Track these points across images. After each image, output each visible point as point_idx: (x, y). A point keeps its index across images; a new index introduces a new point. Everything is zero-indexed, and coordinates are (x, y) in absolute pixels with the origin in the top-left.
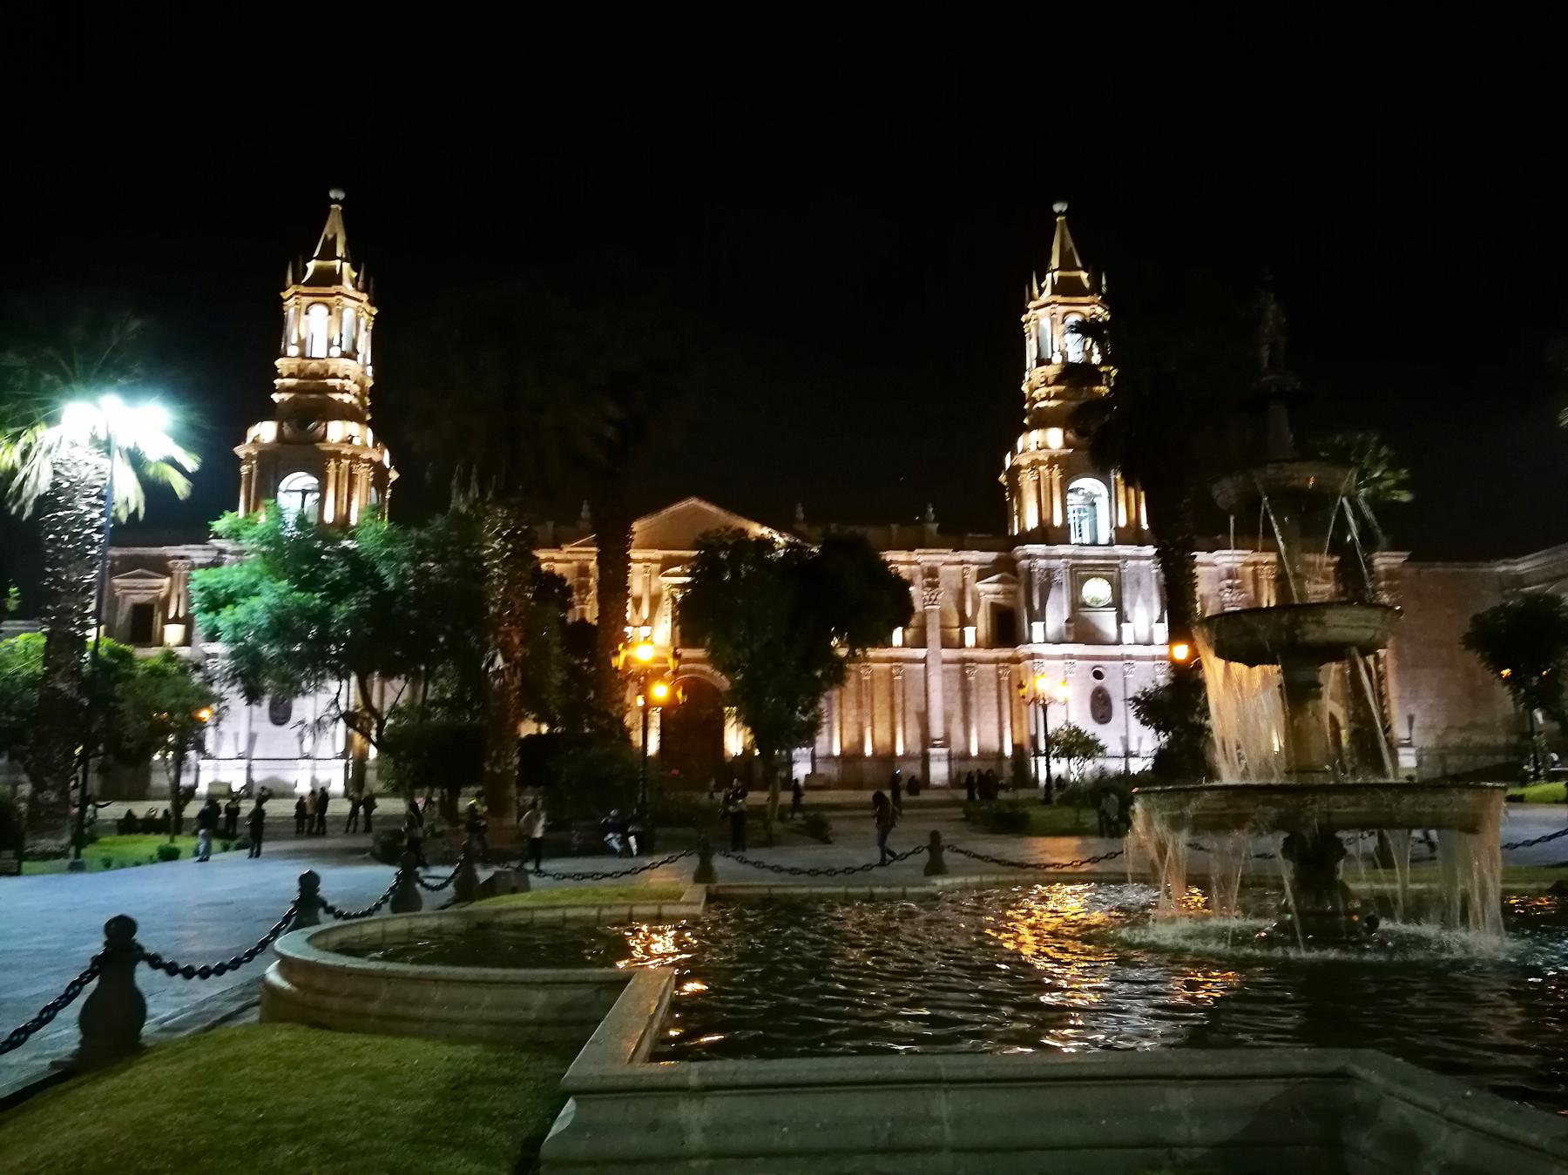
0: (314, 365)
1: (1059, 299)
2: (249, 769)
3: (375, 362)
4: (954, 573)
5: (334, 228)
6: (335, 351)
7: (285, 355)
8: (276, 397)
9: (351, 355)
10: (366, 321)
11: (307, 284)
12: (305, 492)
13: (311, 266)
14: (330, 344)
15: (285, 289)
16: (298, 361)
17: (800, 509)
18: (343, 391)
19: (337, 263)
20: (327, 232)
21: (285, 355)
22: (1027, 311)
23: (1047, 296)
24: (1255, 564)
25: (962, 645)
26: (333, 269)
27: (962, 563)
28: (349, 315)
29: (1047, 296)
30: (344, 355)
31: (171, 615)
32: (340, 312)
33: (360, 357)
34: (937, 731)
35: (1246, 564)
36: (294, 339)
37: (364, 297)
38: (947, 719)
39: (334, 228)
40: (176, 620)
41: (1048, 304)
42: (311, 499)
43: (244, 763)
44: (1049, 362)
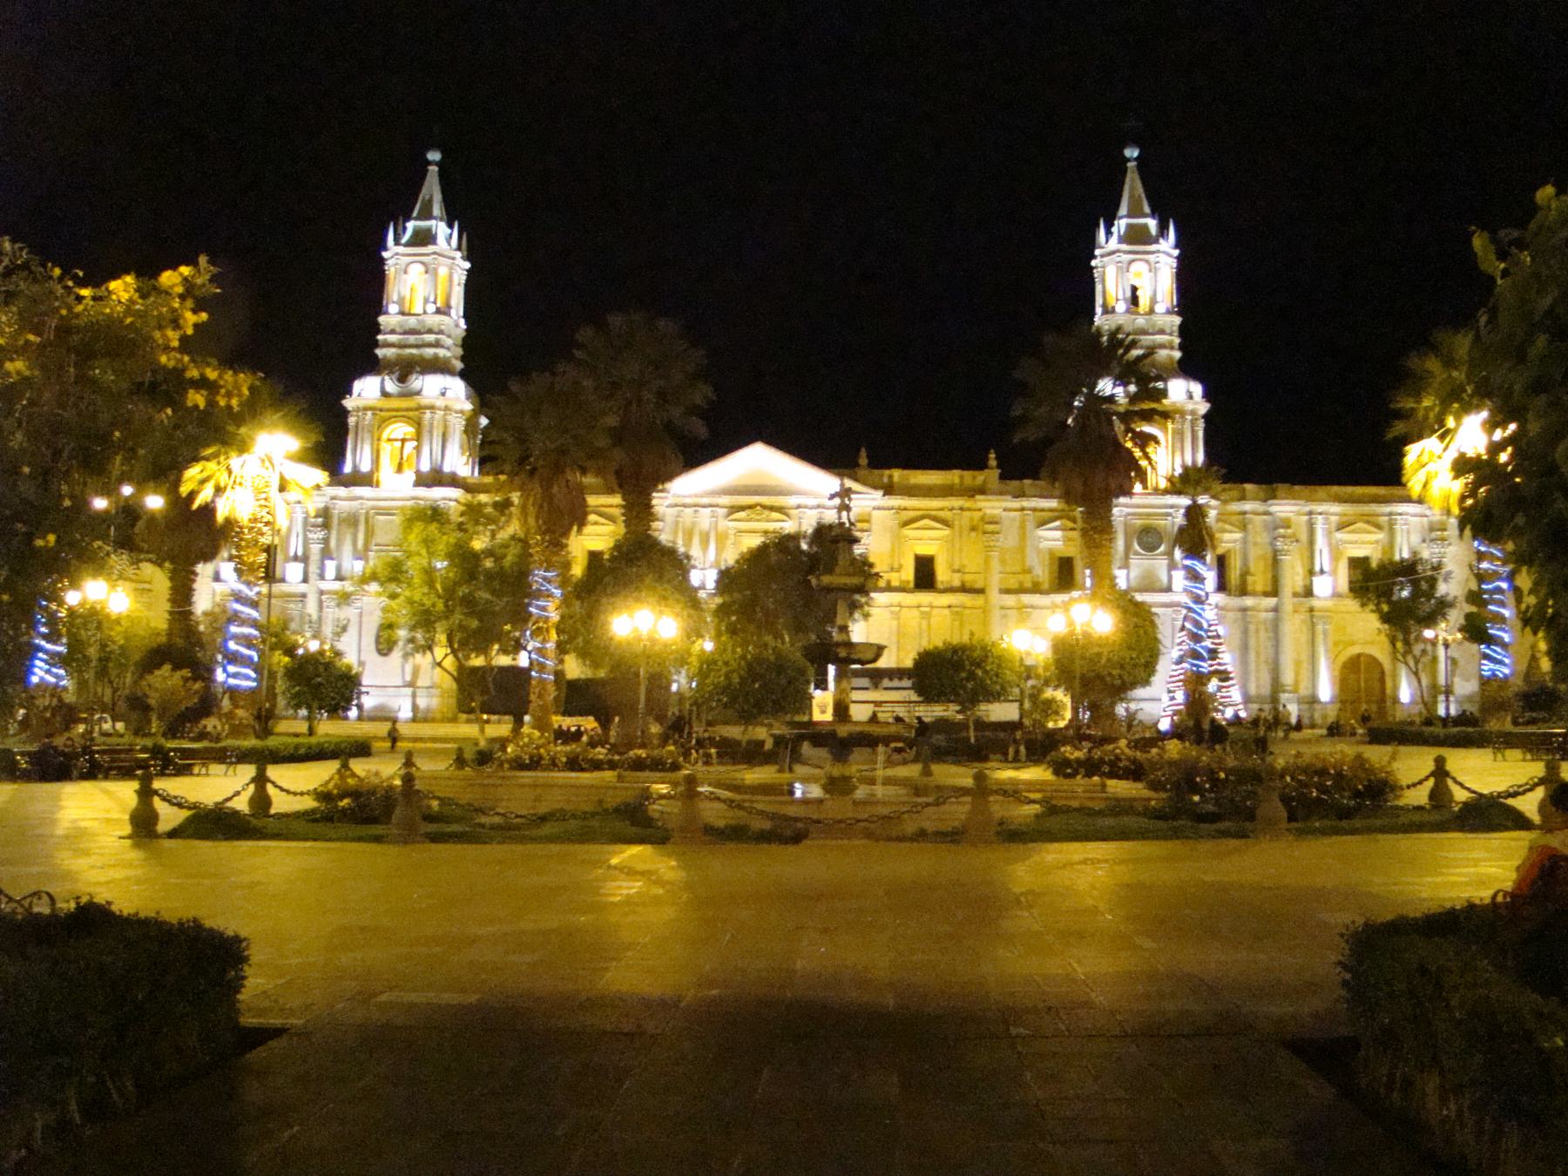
0: (412, 322)
1: (1125, 247)
2: (414, 696)
3: (467, 316)
4: (1014, 519)
5: (432, 188)
6: (431, 308)
7: (386, 313)
8: (380, 352)
9: (443, 311)
10: (460, 277)
11: (408, 244)
12: (403, 441)
13: (411, 225)
14: (426, 301)
15: (386, 249)
16: (401, 318)
17: (992, 456)
18: (437, 344)
19: (433, 223)
20: (424, 193)
21: (386, 313)
22: (1094, 257)
23: (1113, 244)
24: (1310, 513)
25: (1169, 589)
26: (429, 230)
27: (1023, 509)
28: (443, 272)
29: (1113, 244)
30: (438, 311)
31: (292, 554)
32: (436, 270)
33: (453, 312)
34: (1288, 678)
35: (1299, 514)
36: (395, 298)
37: (458, 254)
38: (1298, 663)
39: (432, 188)
40: (296, 558)
41: (1113, 253)
42: (410, 446)
43: (409, 691)
44: (1113, 311)
